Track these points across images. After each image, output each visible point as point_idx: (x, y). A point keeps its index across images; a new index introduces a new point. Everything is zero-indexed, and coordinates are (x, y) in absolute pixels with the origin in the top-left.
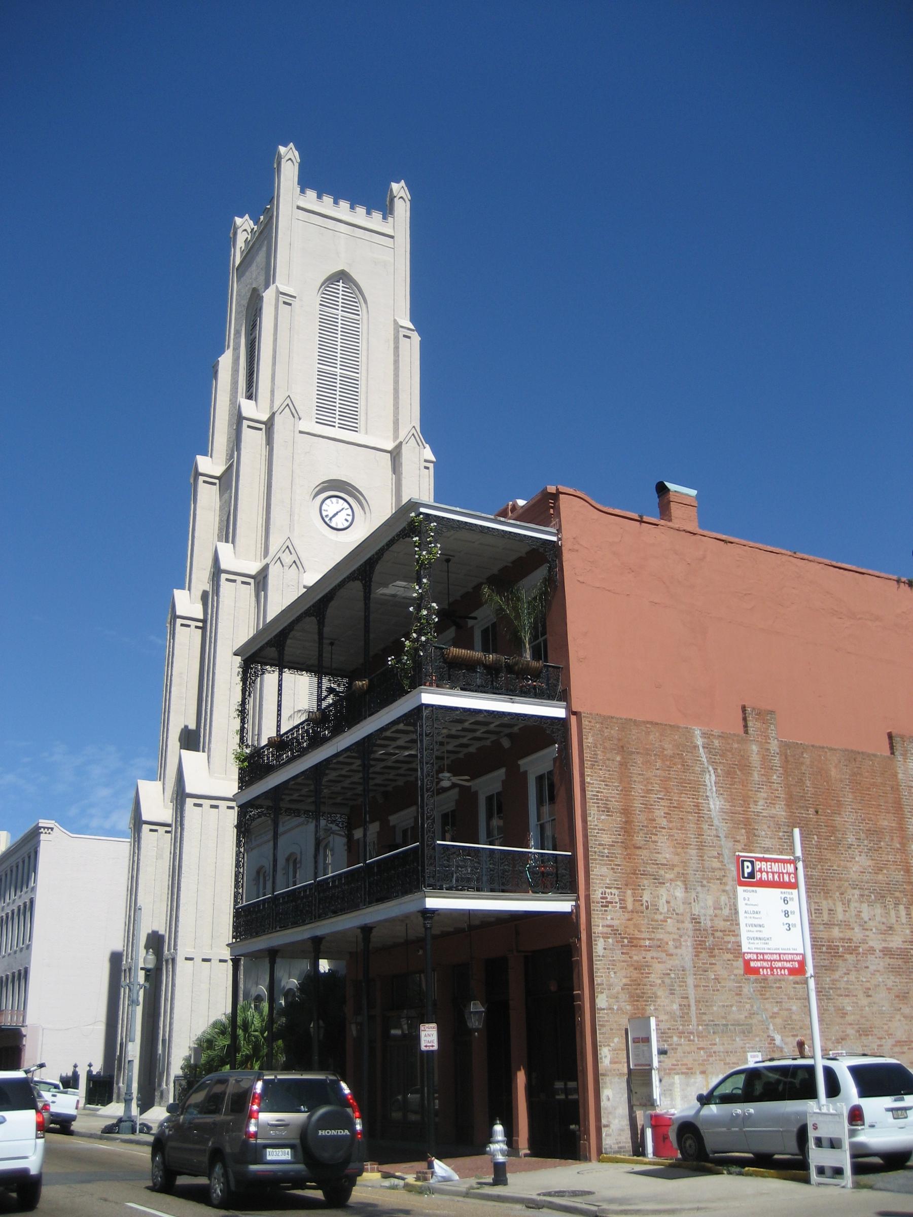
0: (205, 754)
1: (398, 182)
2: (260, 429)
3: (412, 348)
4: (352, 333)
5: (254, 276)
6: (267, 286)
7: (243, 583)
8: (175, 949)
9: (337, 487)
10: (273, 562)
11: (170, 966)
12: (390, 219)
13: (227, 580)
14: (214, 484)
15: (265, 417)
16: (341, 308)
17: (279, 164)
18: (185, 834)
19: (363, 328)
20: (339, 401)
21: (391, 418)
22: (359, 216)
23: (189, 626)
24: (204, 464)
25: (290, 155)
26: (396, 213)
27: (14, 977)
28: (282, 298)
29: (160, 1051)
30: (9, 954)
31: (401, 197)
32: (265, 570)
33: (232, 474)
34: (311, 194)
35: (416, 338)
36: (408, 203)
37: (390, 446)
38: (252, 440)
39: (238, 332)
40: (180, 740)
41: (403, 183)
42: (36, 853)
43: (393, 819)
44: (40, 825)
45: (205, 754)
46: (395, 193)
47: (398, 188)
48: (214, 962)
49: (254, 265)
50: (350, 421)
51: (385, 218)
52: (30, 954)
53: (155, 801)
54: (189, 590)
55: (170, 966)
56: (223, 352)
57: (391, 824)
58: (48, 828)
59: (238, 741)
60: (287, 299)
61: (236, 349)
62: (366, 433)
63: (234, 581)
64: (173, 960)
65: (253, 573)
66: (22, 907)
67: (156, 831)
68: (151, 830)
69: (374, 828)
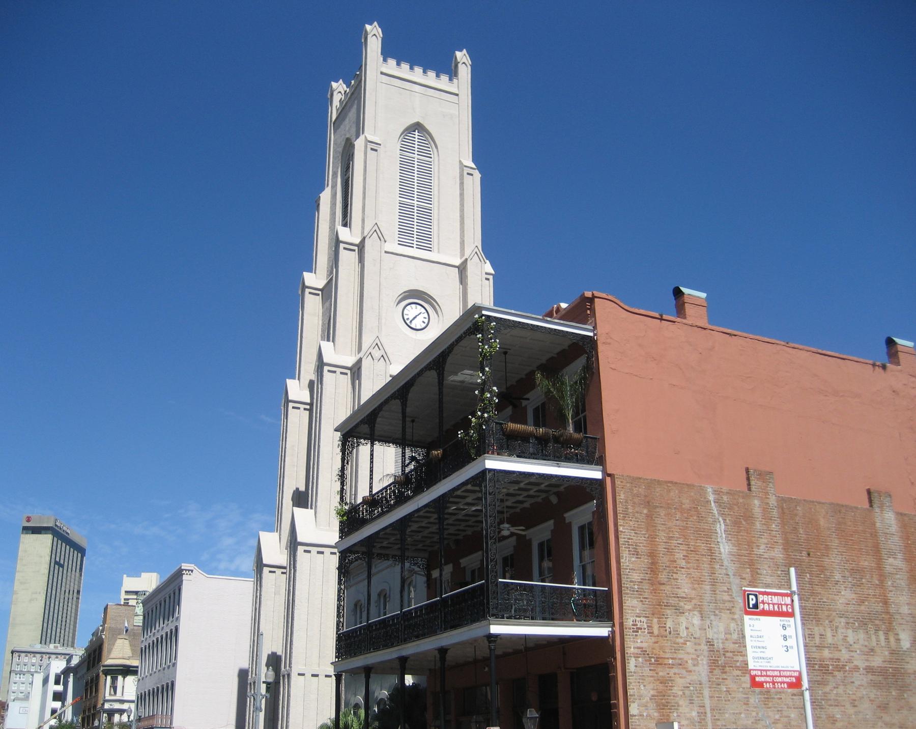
1: (461, 50)
3: (474, 183)
4: (426, 172)
6: (358, 136)
7: (341, 373)
8: (290, 667)
9: (416, 296)
12: (455, 81)
13: (329, 371)
14: (318, 295)
15: (357, 241)
19: (435, 168)
20: (416, 227)
22: (431, 78)
25: (375, 32)
27: (163, 688)
28: (370, 146)
32: (360, 361)
34: (392, 62)
35: (477, 175)
36: (469, 67)
38: (348, 259)
39: (335, 174)
40: (292, 499)
42: (180, 590)
43: (464, 562)
46: (459, 60)
47: (462, 56)
48: (322, 677)
49: (347, 120)
50: (425, 242)
51: (451, 80)
53: (273, 548)
54: (299, 379)
60: (374, 147)
61: (334, 186)
63: (335, 372)
64: (289, 675)
65: (350, 365)
68: (270, 572)
69: (448, 569)
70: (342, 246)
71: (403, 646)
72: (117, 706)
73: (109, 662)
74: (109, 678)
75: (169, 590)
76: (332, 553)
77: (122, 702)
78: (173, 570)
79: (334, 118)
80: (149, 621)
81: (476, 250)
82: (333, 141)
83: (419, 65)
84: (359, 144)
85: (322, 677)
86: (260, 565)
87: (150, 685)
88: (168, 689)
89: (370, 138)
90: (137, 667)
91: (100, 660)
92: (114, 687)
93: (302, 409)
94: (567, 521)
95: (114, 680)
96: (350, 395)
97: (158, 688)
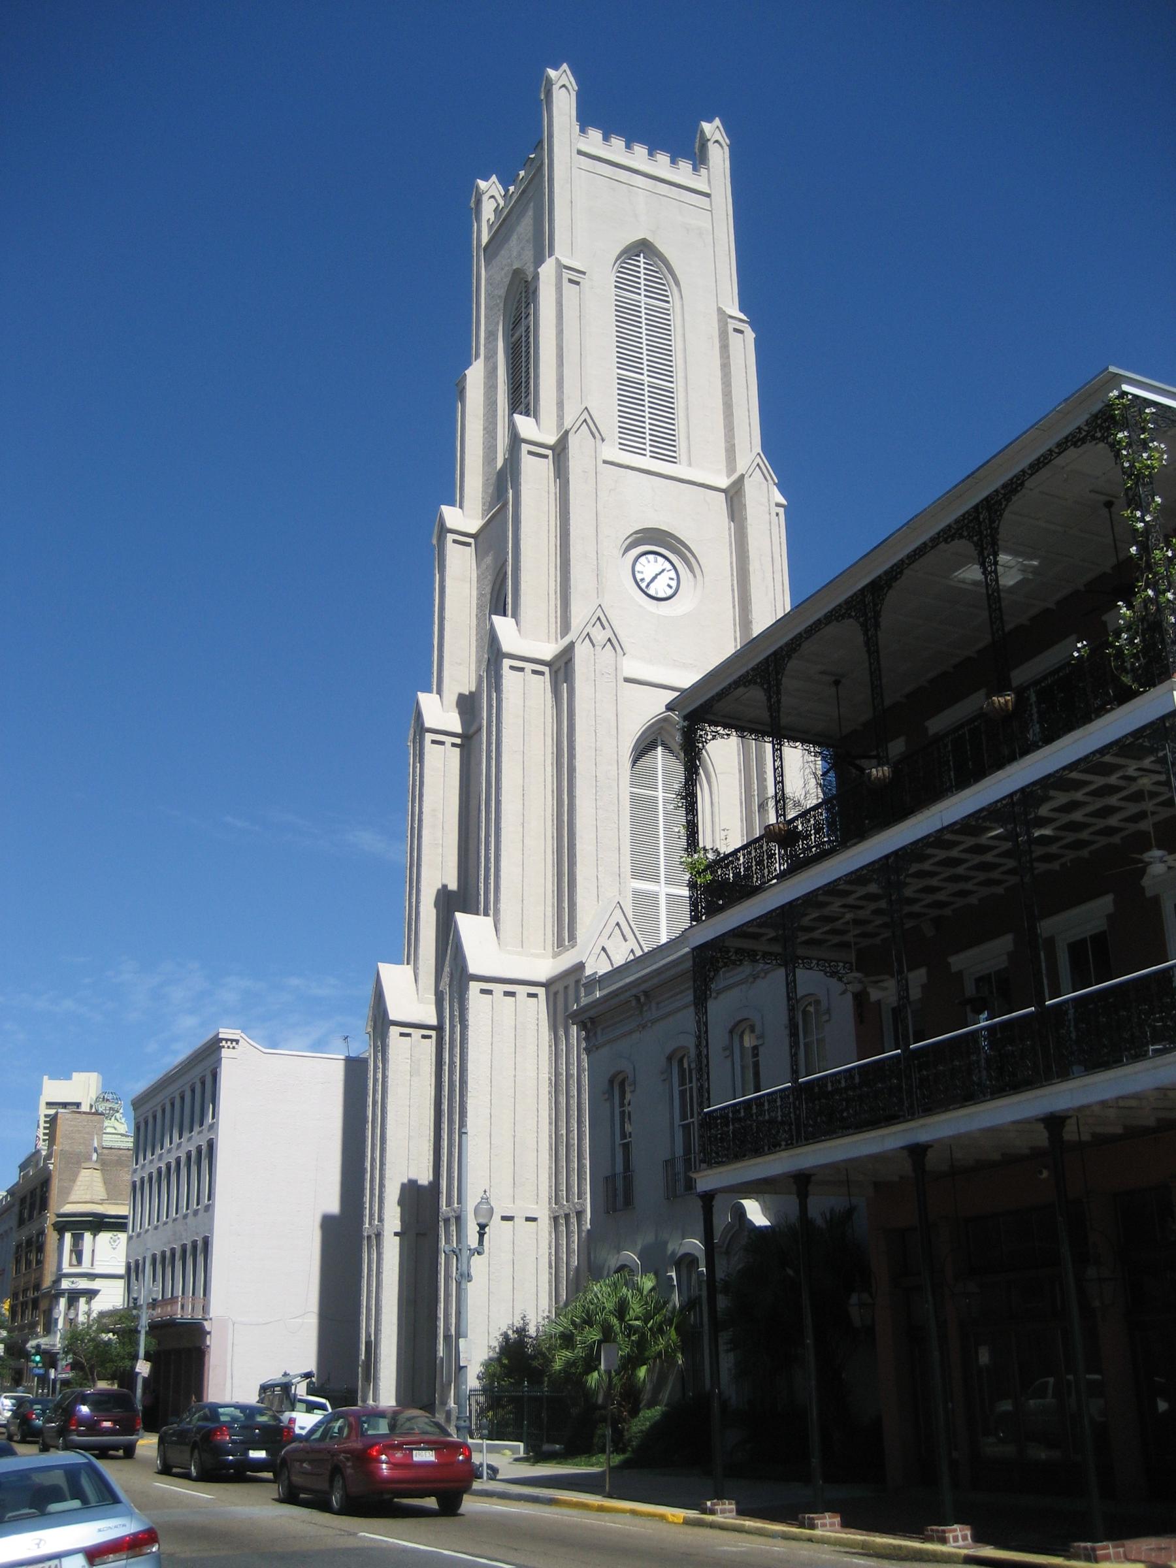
0: (489, 920)
1: (710, 120)
2: (546, 457)
3: (744, 347)
4: (661, 326)
5: (515, 254)
6: (539, 261)
7: (535, 672)
8: (381, 1220)
9: (655, 540)
10: (580, 640)
11: (453, 1228)
12: (703, 171)
13: (512, 668)
14: (468, 545)
15: (551, 440)
16: (643, 293)
17: (549, 94)
18: (471, 1033)
19: (676, 320)
20: (650, 418)
21: (722, 444)
22: (661, 165)
23: (442, 743)
24: (452, 516)
25: (564, 80)
26: (711, 163)
27: (184, 1251)
28: (567, 274)
29: (441, 1354)
30: (175, 1220)
31: (717, 141)
32: (569, 650)
33: (506, 522)
34: (595, 135)
35: (750, 335)
36: (727, 149)
37: (724, 483)
38: (535, 474)
39: (491, 335)
40: (436, 905)
41: (717, 122)
42: (215, 1076)
43: (957, 962)
44: (221, 1036)
45: (489, 920)
46: (708, 135)
47: (712, 129)
48: (520, 1221)
49: (515, 237)
50: (665, 445)
51: (695, 169)
52: (212, 1219)
53: (408, 992)
54: (439, 692)
55: (453, 1228)
56: (470, 364)
57: (954, 969)
58: (232, 1041)
59: (683, 843)
60: (573, 276)
61: (491, 357)
62: (690, 465)
63: (522, 669)
64: (379, 1235)
65: (548, 657)
66: (194, 1154)
67: (409, 1035)
68: (402, 1035)
69: (917, 978)
70: (525, 448)
71: (922, 1121)
72: (83, 1284)
73: (68, 1208)
74: (68, 1236)
75: (195, 1074)
76: (424, 1037)
77: (92, 1277)
78: (211, 1036)
79: (485, 239)
80: (148, 1133)
81: (758, 460)
82: (486, 284)
83: (641, 141)
84: (547, 271)
85: (520, 1221)
86: (381, 1022)
87: (157, 1244)
88: (198, 1251)
89: (566, 261)
90: (125, 1217)
91: (44, 1204)
92: (78, 1253)
93: (448, 745)
94: (1149, 894)
95: (77, 1239)
96: (550, 711)
97: (173, 1251)
